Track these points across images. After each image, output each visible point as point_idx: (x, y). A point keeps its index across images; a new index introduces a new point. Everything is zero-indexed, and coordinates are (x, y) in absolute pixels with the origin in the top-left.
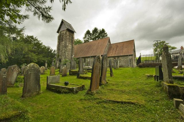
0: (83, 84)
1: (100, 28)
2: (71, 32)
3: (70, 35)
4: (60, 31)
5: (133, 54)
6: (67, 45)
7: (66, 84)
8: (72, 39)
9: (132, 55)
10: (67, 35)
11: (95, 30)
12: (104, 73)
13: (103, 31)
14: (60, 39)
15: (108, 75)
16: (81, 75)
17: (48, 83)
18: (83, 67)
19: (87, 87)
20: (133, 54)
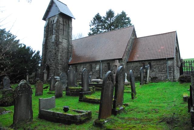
0: (89, 111)
1: (117, 12)
2: (67, 19)
3: (65, 24)
4: (49, 16)
5: (175, 57)
6: (60, 40)
7: (66, 110)
8: (68, 29)
9: (173, 58)
10: (60, 23)
11: (110, 14)
12: (119, 95)
13: (123, 15)
14: (48, 31)
15: (127, 97)
16: (88, 97)
17: (41, 107)
18: (88, 82)
19: (95, 116)
20: (175, 57)
